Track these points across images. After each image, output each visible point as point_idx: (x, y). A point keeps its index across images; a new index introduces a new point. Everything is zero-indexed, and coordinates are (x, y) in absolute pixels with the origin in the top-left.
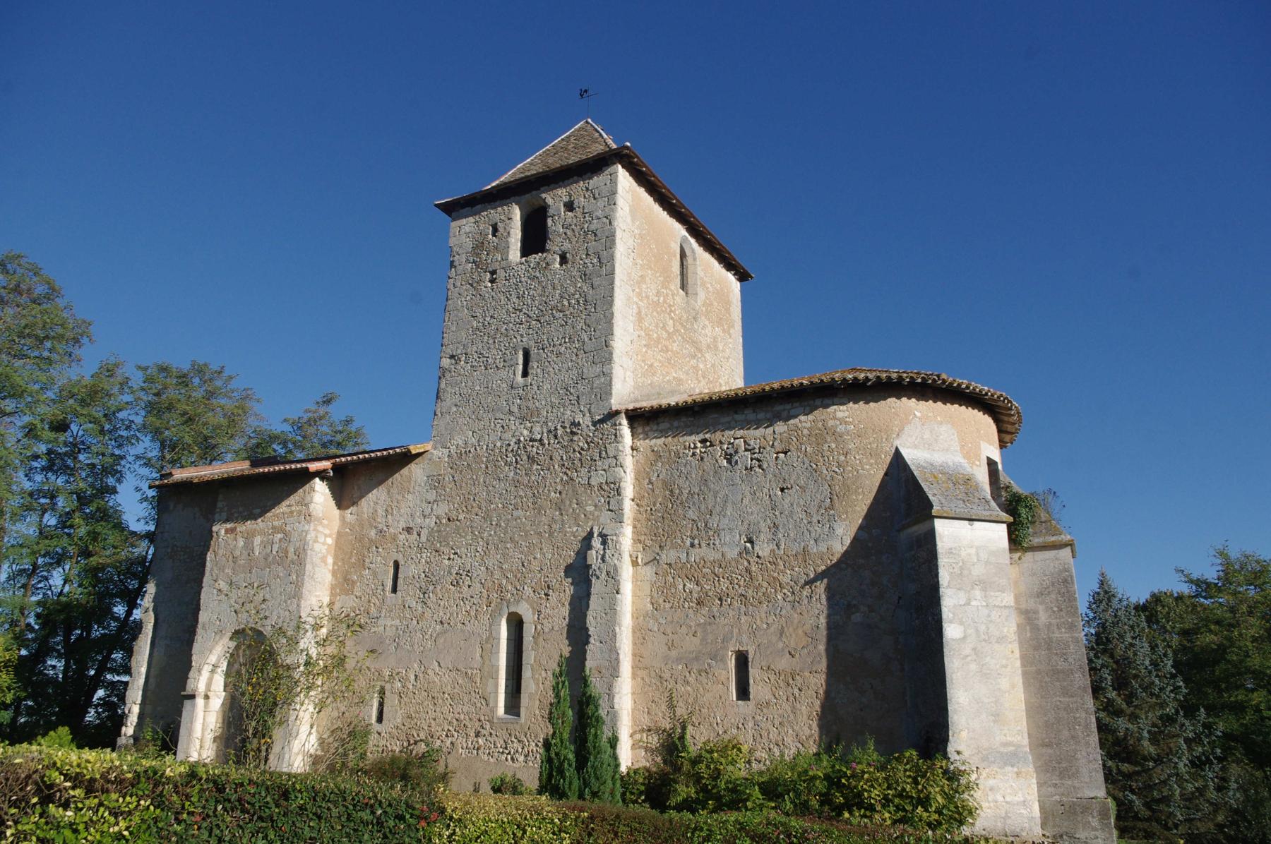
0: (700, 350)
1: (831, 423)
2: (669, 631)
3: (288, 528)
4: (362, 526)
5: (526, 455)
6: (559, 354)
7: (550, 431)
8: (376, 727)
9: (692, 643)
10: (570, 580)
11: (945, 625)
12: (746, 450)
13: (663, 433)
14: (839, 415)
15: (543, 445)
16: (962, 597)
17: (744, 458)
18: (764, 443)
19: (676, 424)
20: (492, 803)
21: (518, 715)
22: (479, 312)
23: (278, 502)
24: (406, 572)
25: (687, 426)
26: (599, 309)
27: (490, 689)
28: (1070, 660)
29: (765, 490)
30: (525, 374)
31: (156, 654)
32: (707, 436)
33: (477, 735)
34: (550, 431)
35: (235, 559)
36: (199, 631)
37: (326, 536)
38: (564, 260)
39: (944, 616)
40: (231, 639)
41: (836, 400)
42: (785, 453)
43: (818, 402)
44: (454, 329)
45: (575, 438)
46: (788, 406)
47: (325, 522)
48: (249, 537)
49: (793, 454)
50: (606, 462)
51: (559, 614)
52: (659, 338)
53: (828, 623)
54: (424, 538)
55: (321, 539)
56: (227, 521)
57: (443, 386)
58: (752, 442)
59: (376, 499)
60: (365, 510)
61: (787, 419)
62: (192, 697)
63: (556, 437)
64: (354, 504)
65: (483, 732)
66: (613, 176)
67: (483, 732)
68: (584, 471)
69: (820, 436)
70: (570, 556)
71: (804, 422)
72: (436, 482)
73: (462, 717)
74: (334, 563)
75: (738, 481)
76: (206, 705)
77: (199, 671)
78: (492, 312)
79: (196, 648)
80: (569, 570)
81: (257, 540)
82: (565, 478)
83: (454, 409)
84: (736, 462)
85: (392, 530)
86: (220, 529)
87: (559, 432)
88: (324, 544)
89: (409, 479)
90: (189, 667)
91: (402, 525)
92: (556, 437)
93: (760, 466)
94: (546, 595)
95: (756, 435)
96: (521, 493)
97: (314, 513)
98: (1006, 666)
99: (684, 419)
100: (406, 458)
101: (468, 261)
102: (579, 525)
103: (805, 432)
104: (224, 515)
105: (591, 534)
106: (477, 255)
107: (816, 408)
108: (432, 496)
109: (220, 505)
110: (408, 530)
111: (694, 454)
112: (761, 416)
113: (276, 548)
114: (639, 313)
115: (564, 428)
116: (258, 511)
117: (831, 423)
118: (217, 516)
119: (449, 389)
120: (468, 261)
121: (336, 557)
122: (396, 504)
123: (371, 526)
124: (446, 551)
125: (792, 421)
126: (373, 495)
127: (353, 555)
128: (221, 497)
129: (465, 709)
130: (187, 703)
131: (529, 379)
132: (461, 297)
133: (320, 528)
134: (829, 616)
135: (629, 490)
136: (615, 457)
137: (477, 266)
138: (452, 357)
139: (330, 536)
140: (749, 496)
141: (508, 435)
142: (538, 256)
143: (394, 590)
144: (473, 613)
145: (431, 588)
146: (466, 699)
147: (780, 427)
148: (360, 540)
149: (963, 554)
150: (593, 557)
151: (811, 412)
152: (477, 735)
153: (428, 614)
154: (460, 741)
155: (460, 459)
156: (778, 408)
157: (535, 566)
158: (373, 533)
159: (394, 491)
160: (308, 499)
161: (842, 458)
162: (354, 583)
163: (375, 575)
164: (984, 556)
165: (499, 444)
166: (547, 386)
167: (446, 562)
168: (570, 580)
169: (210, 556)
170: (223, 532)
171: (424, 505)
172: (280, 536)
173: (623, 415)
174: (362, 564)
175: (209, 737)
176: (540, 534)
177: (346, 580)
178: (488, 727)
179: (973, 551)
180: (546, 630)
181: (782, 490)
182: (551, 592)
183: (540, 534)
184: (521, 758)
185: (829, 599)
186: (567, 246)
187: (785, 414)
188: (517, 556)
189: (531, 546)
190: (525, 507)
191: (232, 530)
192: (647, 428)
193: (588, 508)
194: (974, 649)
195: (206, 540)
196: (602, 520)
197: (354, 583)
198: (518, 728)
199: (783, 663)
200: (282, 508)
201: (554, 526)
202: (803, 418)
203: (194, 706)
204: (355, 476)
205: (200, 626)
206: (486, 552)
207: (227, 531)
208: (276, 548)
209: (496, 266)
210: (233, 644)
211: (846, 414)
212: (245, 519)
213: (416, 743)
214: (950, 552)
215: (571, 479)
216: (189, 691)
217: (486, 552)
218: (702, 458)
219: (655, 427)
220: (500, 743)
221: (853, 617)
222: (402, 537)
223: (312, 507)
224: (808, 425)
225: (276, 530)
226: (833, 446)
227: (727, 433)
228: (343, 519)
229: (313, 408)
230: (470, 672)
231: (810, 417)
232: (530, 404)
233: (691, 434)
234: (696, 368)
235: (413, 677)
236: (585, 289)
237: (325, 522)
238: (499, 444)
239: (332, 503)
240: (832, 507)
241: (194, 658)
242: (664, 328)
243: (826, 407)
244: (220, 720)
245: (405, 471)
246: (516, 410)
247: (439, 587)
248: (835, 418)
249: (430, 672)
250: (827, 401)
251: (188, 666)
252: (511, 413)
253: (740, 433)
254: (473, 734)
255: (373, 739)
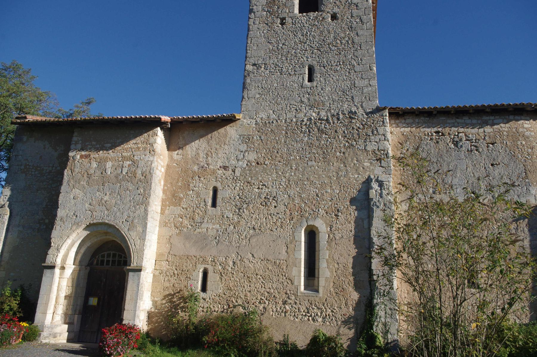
1: (521, 130)
3: (136, 158)
4: (186, 162)
5: (317, 127)
6: (336, 71)
7: (333, 115)
8: (202, 295)
10: (354, 207)
12: (467, 140)
13: (409, 125)
14: (526, 126)
15: (329, 123)
17: (467, 145)
18: (478, 137)
19: (417, 120)
21: (317, 291)
22: (273, 40)
23: (126, 140)
25: (425, 123)
26: (363, 48)
27: (294, 272)
29: (482, 164)
30: (310, 80)
31: (9, 236)
32: (440, 129)
33: (285, 303)
34: (333, 115)
35: (89, 176)
36: (58, 222)
38: (334, 17)
40: (85, 229)
41: (522, 117)
42: (492, 144)
43: (511, 117)
44: (255, 48)
45: (353, 121)
46: (492, 118)
47: (162, 157)
48: (101, 162)
49: (498, 145)
50: (377, 138)
51: (347, 226)
53: (530, 245)
54: (238, 173)
55: (159, 168)
56: (82, 149)
57: (248, 81)
58: (470, 136)
59: (197, 147)
60: (189, 153)
61: (492, 125)
62: (53, 267)
63: (338, 119)
64: (179, 148)
65: (289, 301)
67: (289, 301)
68: (361, 142)
69: (516, 136)
70: (354, 193)
71: (504, 127)
72: (247, 139)
73: (272, 291)
74: (165, 185)
75: (463, 157)
76: (61, 274)
77: (58, 250)
78: (283, 41)
79: (55, 234)
80: (353, 201)
81: (109, 164)
82: (347, 144)
83: (258, 96)
84: (461, 146)
85: (211, 167)
86: (75, 155)
87: (341, 116)
89: (226, 136)
90: (49, 246)
91: (220, 164)
92: (338, 119)
93: (477, 150)
94: (337, 215)
95: (472, 132)
96: (314, 151)
97: (156, 150)
99: (422, 118)
100: (230, 120)
101: (263, 10)
102: (359, 174)
103: (505, 133)
104: (79, 146)
105: (368, 181)
106: (271, 7)
107: (511, 121)
108: (244, 147)
109: (75, 139)
110: (225, 168)
111: (431, 139)
112: (474, 121)
113: (125, 171)
115: (344, 114)
116: (109, 145)
117: (521, 130)
118: (72, 146)
119: (253, 84)
120: (263, 10)
121: (166, 181)
122: (221, 150)
123: (194, 163)
124: (256, 183)
125: (495, 127)
126: (195, 144)
127: (181, 183)
128: (76, 134)
129: (275, 286)
130: (47, 272)
131: (315, 84)
132: (258, 29)
134: (531, 241)
136: (384, 135)
137: (271, 14)
138: (254, 65)
140: (471, 167)
141: (301, 115)
142: (312, 15)
143: (214, 205)
144: (279, 224)
145: (245, 206)
146: (275, 279)
147: (488, 129)
148: (186, 171)
150: (373, 193)
151: (507, 122)
152: (285, 303)
153: (243, 222)
154: (271, 307)
155: (263, 127)
156: (485, 118)
157: (327, 197)
158: (196, 168)
159: (213, 142)
160: (151, 140)
161: (530, 150)
162: (181, 199)
163: (198, 195)
165: (294, 120)
166: (328, 89)
167: (257, 190)
168: (354, 207)
169: (67, 172)
170: (78, 157)
171: (237, 153)
173: (387, 110)
174: (187, 187)
175: (63, 294)
176: (330, 177)
177: (173, 196)
178: (293, 298)
180: (337, 238)
181: (492, 165)
182: (340, 214)
183: (330, 177)
184: (320, 320)
185: (530, 231)
186: (336, 10)
187: (490, 122)
188: (313, 191)
189: (323, 185)
190: (318, 160)
191: (87, 157)
192: (397, 121)
193: (365, 164)
195: (63, 161)
196: (376, 172)
197: (181, 199)
198: (317, 299)
200: (131, 144)
201: (340, 173)
202: (502, 125)
203: (53, 274)
204: (178, 131)
205: (58, 218)
206: (289, 186)
207: (82, 157)
208: (125, 171)
209: (285, 15)
210: (86, 233)
211: (530, 126)
212: (98, 150)
213: (235, 307)
215: (352, 145)
216: (49, 260)
217: (289, 186)
218: (437, 142)
219: (403, 121)
220: (303, 309)
222: (220, 172)
223: (155, 146)
224: (506, 130)
225: (124, 158)
226: (524, 143)
227: (453, 129)
228: (171, 158)
229: (81, 105)
230: (278, 262)
231: (507, 125)
232: (317, 98)
233: (429, 127)
235: (231, 264)
236: (352, 35)
237: (162, 157)
238: (294, 120)
239: (165, 146)
240: (527, 177)
241: (53, 240)
243: (517, 120)
244: (70, 284)
245: (222, 130)
246: (306, 101)
247: (251, 206)
248: (523, 127)
249: (245, 260)
250: (517, 117)
251: (48, 245)
252: (302, 102)
253: (461, 130)
254: (280, 302)
255: (202, 303)
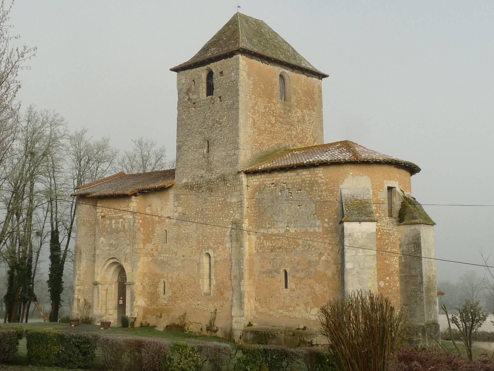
0: (293, 125)
2: (262, 261)
9: (269, 266)
11: (346, 263)
16: (354, 252)
20: (187, 328)
24: (170, 235)
28: (417, 272)
37: (139, 220)
39: (346, 260)
52: (266, 129)
66: (237, 59)
88: (138, 223)
98: (371, 278)
114: (254, 121)
133: (136, 217)
135: (246, 204)
139: (141, 219)
149: (355, 235)
164: (365, 236)
172: (122, 220)
179: (360, 234)
194: (357, 272)
199: (300, 275)
214: (350, 235)
221: (322, 258)
234: (290, 135)
242: (269, 123)
